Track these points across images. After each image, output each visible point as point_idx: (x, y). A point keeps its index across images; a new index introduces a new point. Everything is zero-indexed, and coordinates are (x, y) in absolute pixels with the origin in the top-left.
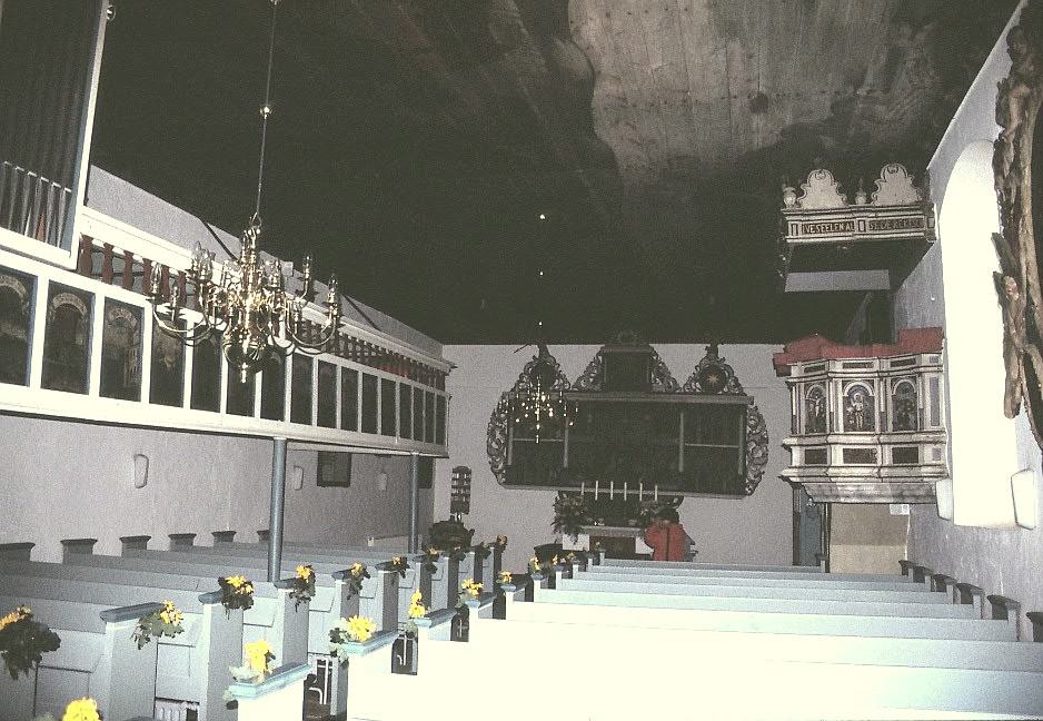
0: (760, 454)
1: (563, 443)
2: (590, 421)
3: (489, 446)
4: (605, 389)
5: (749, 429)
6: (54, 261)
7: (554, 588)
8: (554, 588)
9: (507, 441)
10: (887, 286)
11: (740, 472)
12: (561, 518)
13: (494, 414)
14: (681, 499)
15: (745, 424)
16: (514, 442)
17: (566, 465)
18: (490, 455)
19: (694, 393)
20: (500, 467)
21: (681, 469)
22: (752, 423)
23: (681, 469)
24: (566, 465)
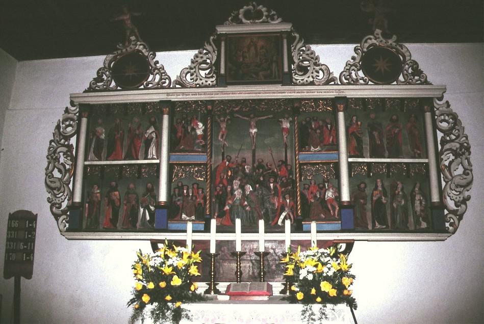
0: (460, 170)
1: (158, 166)
2: (199, 132)
3: (49, 175)
4: (222, 81)
5: (440, 135)
6: (93, 241)
7: (193, 232)
8: (193, 232)
9: (75, 165)
10: (146, 302)
11: (435, 198)
12: (144, 290)
13: (58, 127)
14: (350, 245)
15: (435, 127)
16: (85, 167)
17: (163, 197)
18: (50, 188)
19: (356, 82)
20: (64, 205)
21: (346, 197)
22: (444, 125)
23: (346, 197)
24: (163, 197)
